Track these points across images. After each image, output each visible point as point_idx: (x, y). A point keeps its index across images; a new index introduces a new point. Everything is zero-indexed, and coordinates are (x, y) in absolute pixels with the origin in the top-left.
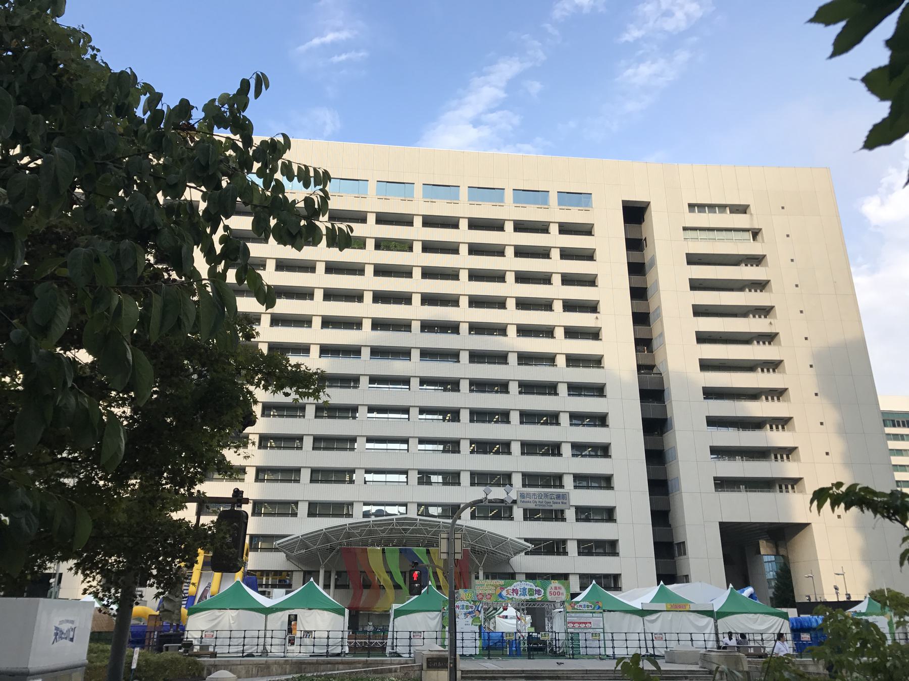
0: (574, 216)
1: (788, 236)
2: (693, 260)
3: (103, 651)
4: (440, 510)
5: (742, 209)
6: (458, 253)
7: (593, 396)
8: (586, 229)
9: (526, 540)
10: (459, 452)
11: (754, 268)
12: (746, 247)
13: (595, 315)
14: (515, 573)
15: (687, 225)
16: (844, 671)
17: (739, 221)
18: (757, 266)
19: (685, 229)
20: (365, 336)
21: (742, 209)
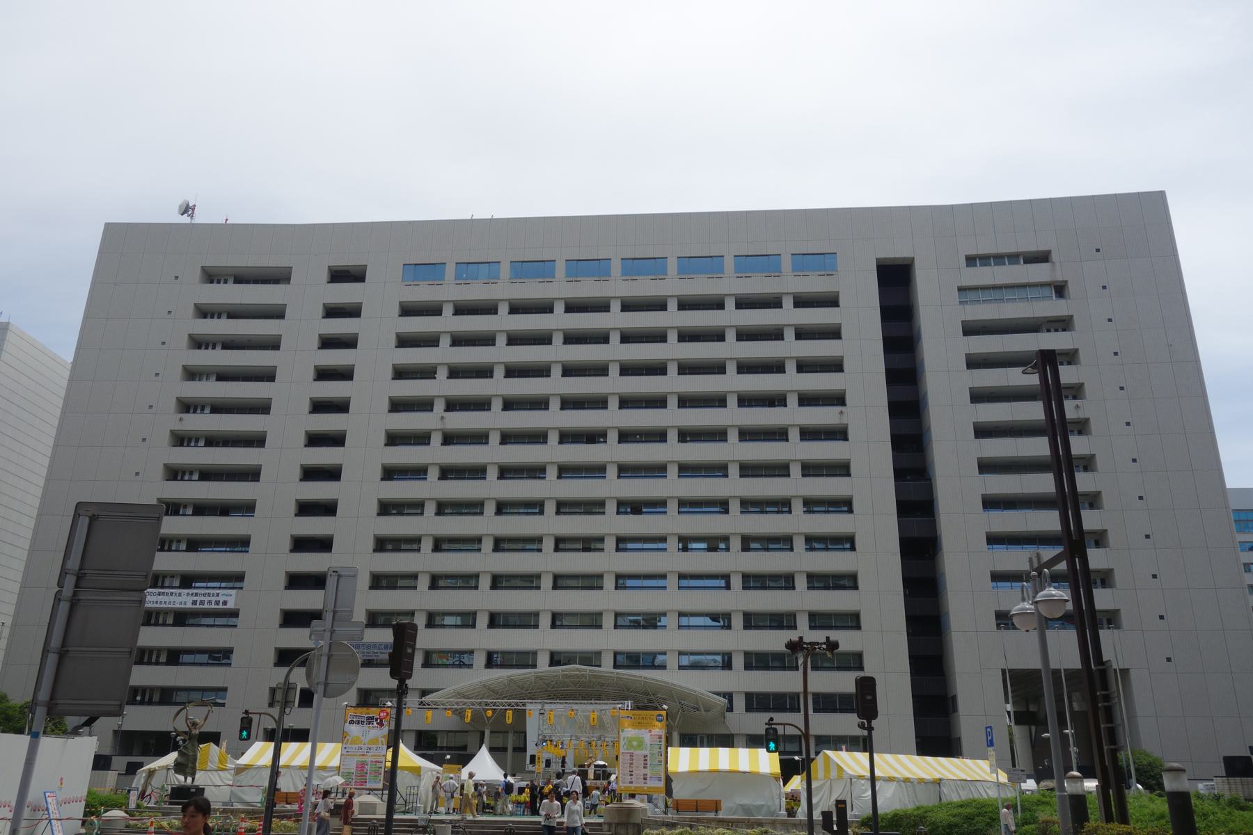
0: (814, 284)
1: (1104, 287)
2: (970, 329)
3: (405, 812)
4: (719, 658)
5: (1042, 257)
6: (840, 338)
7: (580, 513)
8: (971, 295)
9: (718, 694)
10: (793, 588)
11: (1061, 334)
12: (1052, 308)
13: (839, 408)
14: (732, 735)
15: (964, 284)
16: (177, 823)
17: (1038, 273)
18: (1064, 330)
19: (960, 289)
20: (734, 451)
21: (1042, 257)
